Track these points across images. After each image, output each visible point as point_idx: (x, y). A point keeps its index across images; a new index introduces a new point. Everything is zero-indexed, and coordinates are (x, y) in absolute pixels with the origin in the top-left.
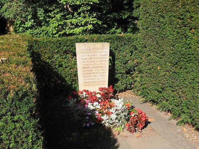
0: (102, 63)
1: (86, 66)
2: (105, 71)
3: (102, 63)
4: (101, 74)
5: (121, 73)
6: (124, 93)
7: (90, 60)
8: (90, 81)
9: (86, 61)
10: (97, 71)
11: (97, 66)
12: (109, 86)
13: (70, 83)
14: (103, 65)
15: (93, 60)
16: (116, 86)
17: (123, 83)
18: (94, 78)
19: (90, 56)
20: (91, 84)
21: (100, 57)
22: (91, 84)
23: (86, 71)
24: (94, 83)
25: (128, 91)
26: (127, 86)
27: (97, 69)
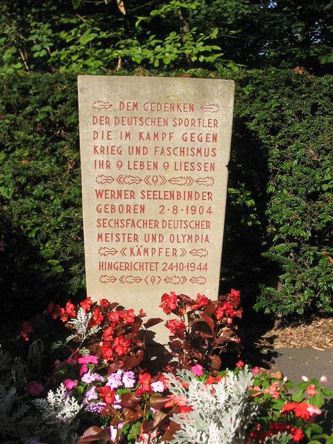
0: (195, 175)
1: (115, 186)
2: (205, 216)
3: (195, 175)
4: (188, 231)
5: (291, 239)
6: (302, 328)
7: (134, 157)
8: (129, 259)
9: (113, 160)
10: (169, 215)
11: (169, 187)
12: (224, 289)
13: (60, 269)
14: (200, 189)
15: (150, 157)
16: (269, 296)
17: (299, 285)
18: (150, 245)
19: (135, 136)
20: (135, 274)
21: (182, 144)
22: (135, 274)
23: (113, 207)
24: (150, 274)
25: (320, 323)
26: (315, 300)
27: (169, 204)
